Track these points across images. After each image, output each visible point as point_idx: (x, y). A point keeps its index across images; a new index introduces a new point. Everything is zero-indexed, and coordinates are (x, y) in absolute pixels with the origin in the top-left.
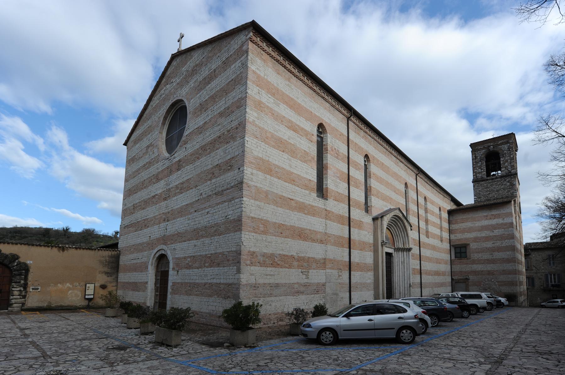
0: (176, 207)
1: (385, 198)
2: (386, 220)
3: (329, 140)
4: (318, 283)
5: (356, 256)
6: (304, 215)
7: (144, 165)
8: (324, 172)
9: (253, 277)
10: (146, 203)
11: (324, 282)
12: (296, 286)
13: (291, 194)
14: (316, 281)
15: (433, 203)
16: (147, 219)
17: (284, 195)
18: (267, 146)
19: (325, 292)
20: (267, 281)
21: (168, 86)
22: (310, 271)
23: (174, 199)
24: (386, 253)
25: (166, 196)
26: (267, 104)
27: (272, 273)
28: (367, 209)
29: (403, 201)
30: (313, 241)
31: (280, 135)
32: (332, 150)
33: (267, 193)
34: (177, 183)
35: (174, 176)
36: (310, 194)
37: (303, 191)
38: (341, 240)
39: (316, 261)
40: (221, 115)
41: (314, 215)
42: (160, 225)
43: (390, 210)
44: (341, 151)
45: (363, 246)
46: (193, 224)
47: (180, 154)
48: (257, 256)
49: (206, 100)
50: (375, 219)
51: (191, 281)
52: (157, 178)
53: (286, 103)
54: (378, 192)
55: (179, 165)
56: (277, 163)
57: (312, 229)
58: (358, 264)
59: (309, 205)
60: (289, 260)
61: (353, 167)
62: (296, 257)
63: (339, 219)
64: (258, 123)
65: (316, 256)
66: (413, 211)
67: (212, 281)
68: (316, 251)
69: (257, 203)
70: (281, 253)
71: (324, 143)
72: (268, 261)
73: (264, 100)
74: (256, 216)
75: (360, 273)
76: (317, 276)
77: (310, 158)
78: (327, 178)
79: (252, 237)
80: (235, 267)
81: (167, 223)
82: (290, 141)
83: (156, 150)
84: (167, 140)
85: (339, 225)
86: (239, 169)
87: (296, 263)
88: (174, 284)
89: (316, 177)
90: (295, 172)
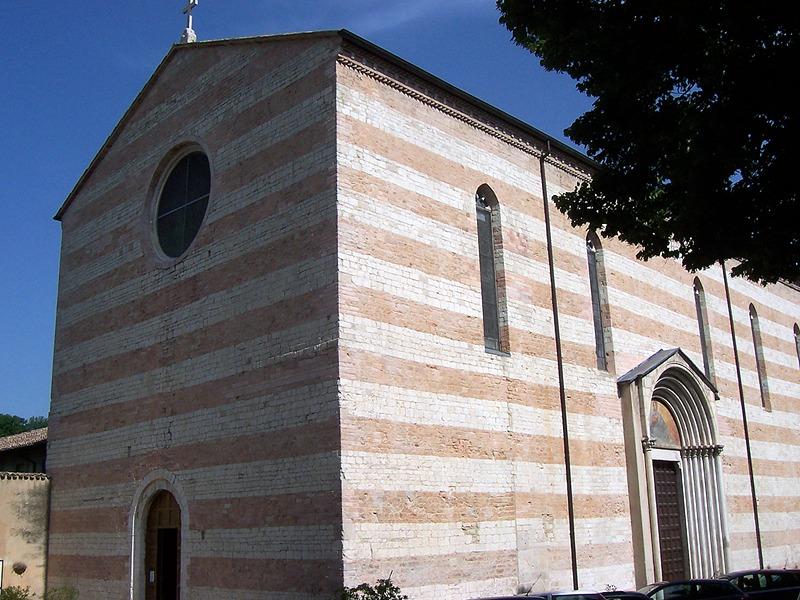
0: (192, 383)
1: (647, 328)
2: (650, 383)
3: (503, 218)
4: (501, 552)
5: (585, 481)
6: (459, 398)
7: (109, 275)
8: (499, 290)
9: (367, 545)
10: (121, 365)
11: (514, 547)
12: (453, 561)
13: (432, 355)
14: (495, 548)
15: (774, 316)
16: (120, 405)
17: (418, 359)
18: (379, 261)
19: (516, 572)
20: (393, 554)
21: (164, 107)
22: (482, 525)
23: (185, 364)
24: (657, 464)
25: (166, 354)
26: (375, 175)
27: (403, 535)
28: (604, 358)
29: (693, 327)
30: (484, 454)
31: (400, 231)
32: (512, 239)
33: (383, 362)
34: (194, 328)
35: (184, 313)
36: (470, 348)
37: (456, 343)
38: (547, 446)
39: (493, 501)
40: (287, 195)
41: (481, 395)
42: (155, 422)
43: (660, 357)
44: (532, 236)
45: (599, 454)
46: (233, 425)
47: (194, 263)
48: (371, 499)
49: (252, 158)
50: (622, 386)
51: (236, 555)
52: (142, 310)
53: (409, 161)
54: (627, 314)
55: (193, 290)
56: (399, 293)
57: (481, 428)
58: (589, 498)
59: (471, 373)
60: (435, 504)
61: (561, 267)
62: (450, 495)
63: (538, 396)
64: (359, 219)
65: (491, 490)
66: (722, 347)
67: (282, 556)
68: (489, 477)
69: (368, 386)
70: (418, 488)
71: (494, 225)
72: (395, 510)
73: (368, 169)
74: (366, 415)
75: (595, 520)
76: (497, 536)
77: (465, 268)
78: (504, 303)
79: (360, 461)
80: (331, 526)
81: (171, 419)
82: (422, 240)
83: (137, 244)
84: (160, 221)
85: (539, 410)
86: (329, 317)
87: (449, 510)
88: (195, 561)
89: (480, 308)
90: (436, 304)
